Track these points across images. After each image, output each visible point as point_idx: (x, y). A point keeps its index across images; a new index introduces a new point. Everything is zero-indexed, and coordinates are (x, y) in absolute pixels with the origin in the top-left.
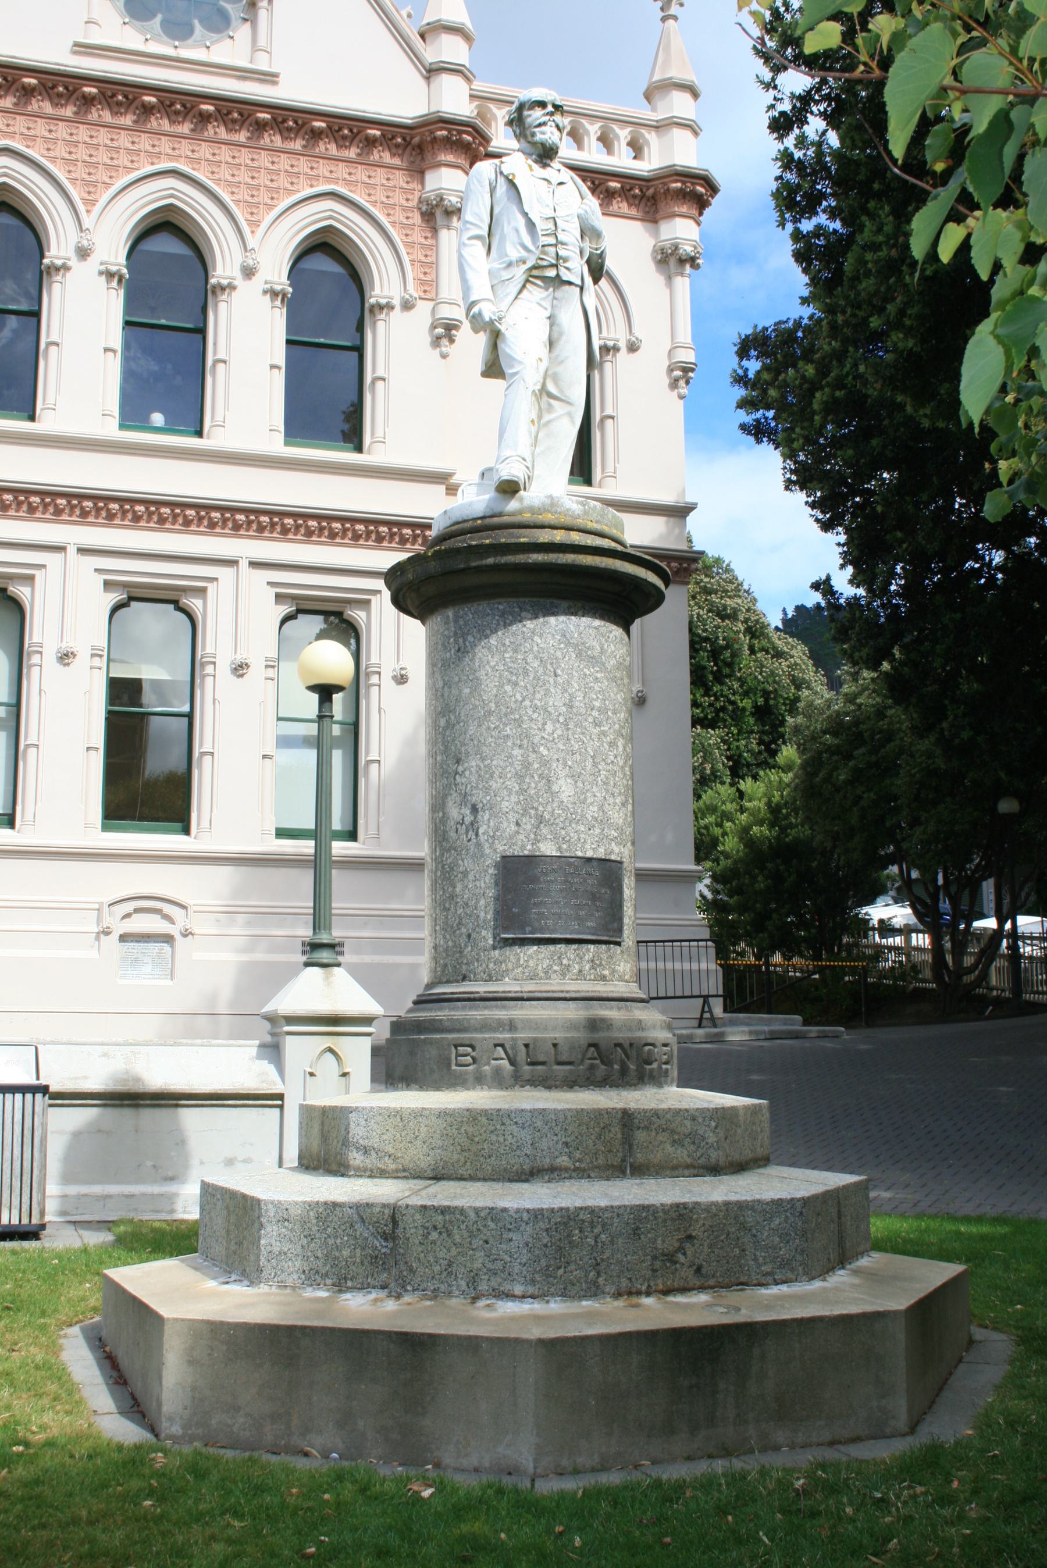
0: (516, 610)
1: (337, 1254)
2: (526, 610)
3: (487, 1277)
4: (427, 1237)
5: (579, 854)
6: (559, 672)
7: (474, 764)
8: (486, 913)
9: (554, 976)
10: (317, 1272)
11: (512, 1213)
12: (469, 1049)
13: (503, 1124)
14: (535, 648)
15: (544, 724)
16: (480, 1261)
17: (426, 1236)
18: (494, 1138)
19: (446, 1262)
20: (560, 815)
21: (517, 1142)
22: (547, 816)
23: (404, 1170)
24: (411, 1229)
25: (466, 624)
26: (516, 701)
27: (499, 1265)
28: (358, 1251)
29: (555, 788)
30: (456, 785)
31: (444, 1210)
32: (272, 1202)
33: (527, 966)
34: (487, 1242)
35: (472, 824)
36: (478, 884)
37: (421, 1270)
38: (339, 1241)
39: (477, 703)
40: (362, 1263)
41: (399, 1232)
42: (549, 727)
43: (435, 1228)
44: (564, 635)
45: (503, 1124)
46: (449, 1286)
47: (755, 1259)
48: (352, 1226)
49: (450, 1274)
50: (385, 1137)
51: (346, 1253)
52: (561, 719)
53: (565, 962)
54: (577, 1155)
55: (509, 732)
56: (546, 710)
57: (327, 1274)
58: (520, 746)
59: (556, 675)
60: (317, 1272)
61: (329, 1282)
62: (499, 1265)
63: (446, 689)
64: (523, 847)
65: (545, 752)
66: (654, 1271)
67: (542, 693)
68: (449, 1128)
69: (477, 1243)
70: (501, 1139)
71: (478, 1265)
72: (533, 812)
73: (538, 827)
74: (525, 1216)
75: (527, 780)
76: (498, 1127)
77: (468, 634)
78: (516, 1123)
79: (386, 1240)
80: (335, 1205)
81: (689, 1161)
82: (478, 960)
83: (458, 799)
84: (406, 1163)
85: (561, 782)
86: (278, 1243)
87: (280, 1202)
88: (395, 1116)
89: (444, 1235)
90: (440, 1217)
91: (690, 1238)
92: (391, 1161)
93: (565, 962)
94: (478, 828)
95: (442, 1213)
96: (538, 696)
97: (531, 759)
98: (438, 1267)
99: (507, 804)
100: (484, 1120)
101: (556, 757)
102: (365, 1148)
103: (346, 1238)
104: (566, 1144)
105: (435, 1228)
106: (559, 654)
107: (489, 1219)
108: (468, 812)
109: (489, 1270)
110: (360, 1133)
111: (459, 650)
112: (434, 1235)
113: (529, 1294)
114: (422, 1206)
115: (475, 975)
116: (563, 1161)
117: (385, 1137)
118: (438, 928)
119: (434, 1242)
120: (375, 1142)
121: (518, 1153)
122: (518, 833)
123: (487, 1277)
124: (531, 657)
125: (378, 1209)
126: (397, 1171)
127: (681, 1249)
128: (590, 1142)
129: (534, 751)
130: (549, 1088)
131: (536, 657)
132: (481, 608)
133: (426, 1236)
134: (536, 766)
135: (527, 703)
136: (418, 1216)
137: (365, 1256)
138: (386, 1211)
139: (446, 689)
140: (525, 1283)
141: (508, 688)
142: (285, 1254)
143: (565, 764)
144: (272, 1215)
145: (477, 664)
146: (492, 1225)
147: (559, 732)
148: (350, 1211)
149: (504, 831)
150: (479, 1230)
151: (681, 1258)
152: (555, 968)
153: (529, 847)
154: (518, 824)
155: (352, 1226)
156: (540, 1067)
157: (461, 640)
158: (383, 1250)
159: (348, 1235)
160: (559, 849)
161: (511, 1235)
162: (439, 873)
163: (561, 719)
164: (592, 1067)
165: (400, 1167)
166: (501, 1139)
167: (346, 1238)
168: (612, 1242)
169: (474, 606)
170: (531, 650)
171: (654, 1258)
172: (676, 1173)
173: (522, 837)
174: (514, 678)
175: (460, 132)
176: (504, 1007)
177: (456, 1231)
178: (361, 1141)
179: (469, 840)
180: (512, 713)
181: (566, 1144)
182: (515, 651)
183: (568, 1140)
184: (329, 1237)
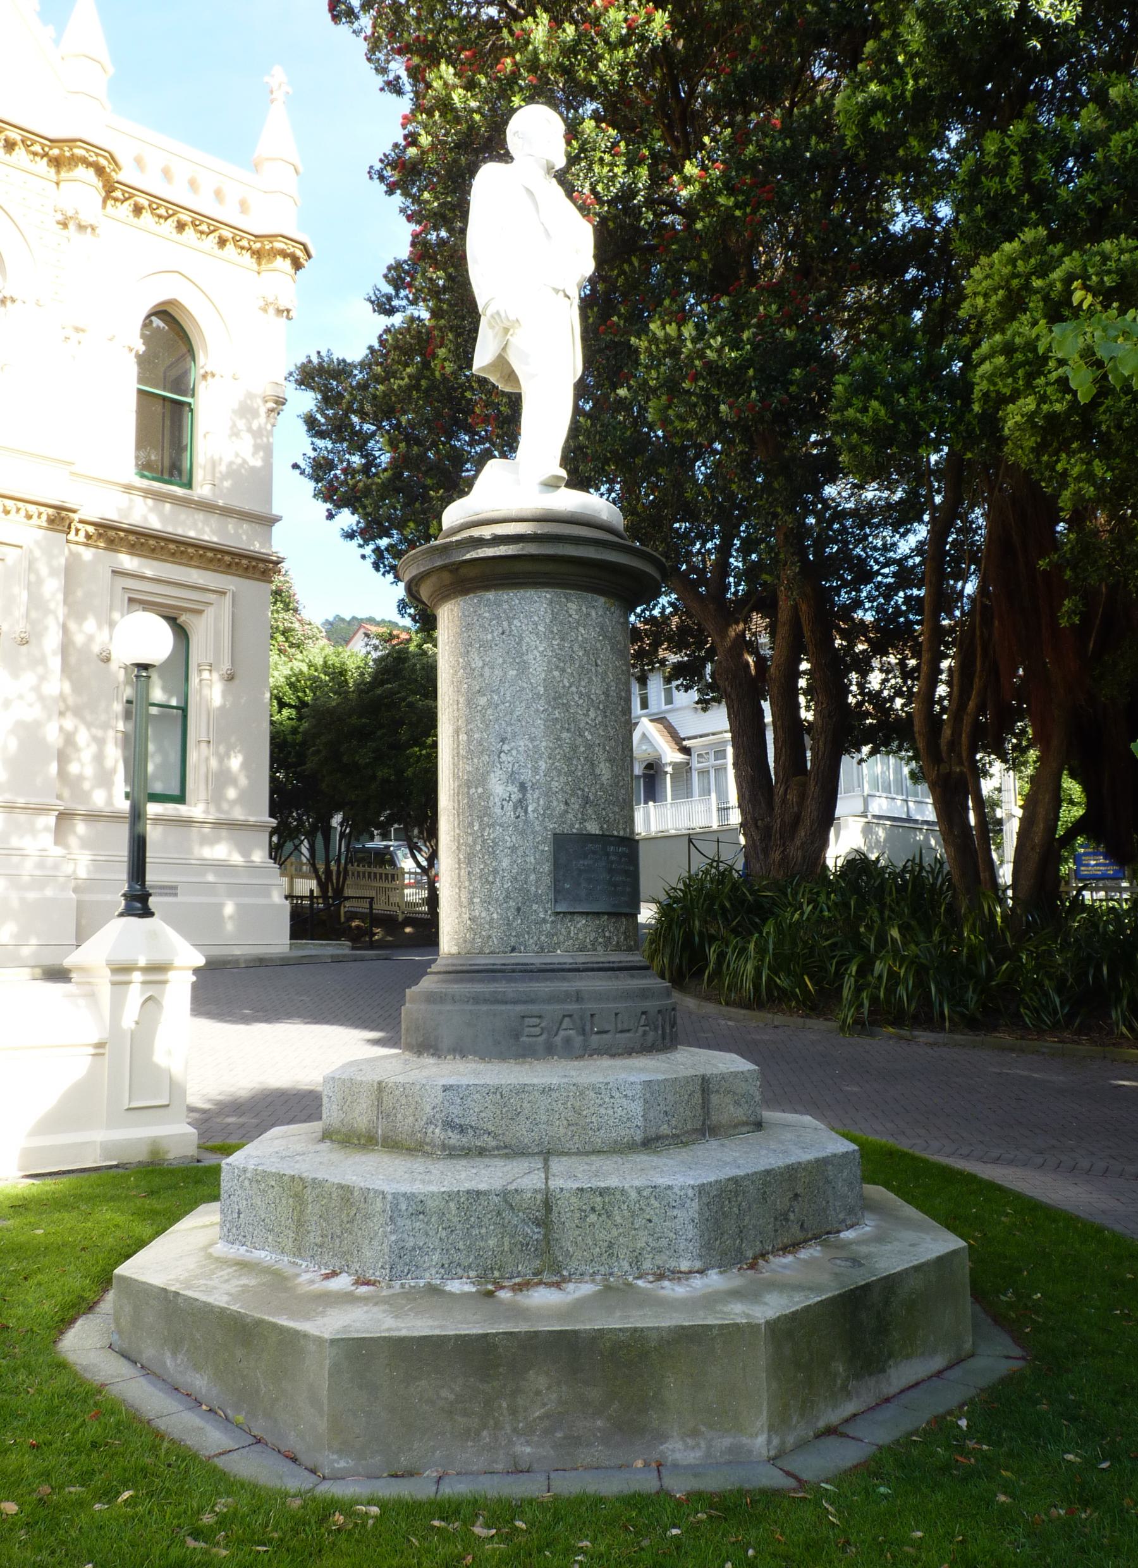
0: (563, 600)
1: (482, 1244)
2: (571, 601)
3: (651, 1256)
4: (585, 1220)
5: (615, 833)
6: (599, 662)
7: (522, 743)
8: (537, 887)
9: (599, 948)
10: (459, 1265)
11: (676, 1190)
12: (537, 1021)
13: (612, 1097)
14: (580, 638)
15: (588, 710)
16: (644, 1239)
17: (583, 1219)
18: (603, 1111)
19: (606, 1244)
20: (601, 797)
21: (627, 1114)
22: (592, 797)
23: (506, 1147)
24: (566, 1212)
25: (512, 608)
26: (564, 686)
27: (664, 1243)
28: (506, 1239)
29: (598, 771)
30: (500, 763)
31: (603, 1192)
32: (404, 1195)
33: (577, 939)
34: (650, 1221)
35: (520, 801)
36: (528, 859)
37: (579, 1254)
38: (483, 1231)
39: (525, 685)
40: (511, 1252)
41: (554, 1217)
42: (592, 714)
43: (593, 1209)
44: (602, 628)
45: (612, 1097)
46: (610, 1268)
47: (835, 1210)
48: (499, 1214)
49: (611, 1255)
50: (483, 1115)
51: (492, 1242)
52: (601, 707)
53: (607, 934)
54: (674, 1123)
55: (557, 715)
56: (589, 697)
57: (469, 1266)
58: (568, 730)
59: (597, 665)
60: (459, 1265)
61: (472, 1274)
62: (664, 1243)
63: (486, 669)
64: (572, 826)
65: (589, 737)
66: (776, 1231)
67: (586, 680)
68: (554, 1104)
69: (639, 1222)
70: (610, 1112)
71: (641, 1244)
72: (580, 792)
73: (584, 807)
74: (690, 1192)
75: (575, 762)
76: (607, 1100)
77: (514, 618)
78: (626, 1096)
79: (538, 1225)
80: (478, 1193)
81: (744, 1119)
82: (528, 933)
83: (504, 777)
84: (507, 1139)
85: (602, 765)
86: (412, 1239)
87: (413, 1194)
88: (495, 1093)
89: (604, 1217)
90: (599, 1199)
91: (796, 1195)
92: (490, 1138)
93: (607, 934)
94: (527, 806)
95: (601, 1195)
96: (583, 683)
97: (577, 743)
98: (598, 1249)
99: (556, 784)
100: (592, 1095)
101: (597, 742)
102: (461, 1126)
103: (492, 1227)
104: (666, 1112)
105: (593, 1209)
106: (598, 645)
107: (652, 1199)
108: (516, 790)
109: (653, 1248)
110: (456, 1112)
111: (503, 633)
112: (593, 1218)
113: (696, 1269)
114: (578, 1189)
115: (525, 947)
116: (665, 1129)
117: (483, 1115)
118: (477, 900)
119: (592, 1225)
120: (472, 1120)
121: (628, 1125)
122: (567, 812)
123: (651, 1256)
124: (576, 646)
125: (529, 1196)
126: (498, 1148)
127: (791, 1209)
128: (682, 1110)
129: (580, 735)
130: (613, 1056)
131: (581, 647)
132: (528, 595)
133: (583, 1219)
134: (582, 749)
135: (574, 689)
136: (573, 1200)
137: (515, 1244)
138: (539, 1197)
139: (486, 669)
140: (692, 1259)
141: (556, 673)
142: (420, 1248)
143: (604, 749)
144: (404, 1208)
145: (524, 648)
146: (656, 1204)
147: (600, 719)
148: (496, 1199)
149: (554, 810)
150: (641, 1209)
151: (792, 1216)
152: (600, 940)
153: (577, 826)
154: (567, 804)
155: (499, 1214)
156: (605, 1036)
157: (505, 624)
158: (535, 1237)
159: (495, 1224)
160: (601, 828)
161: (675, 1212)
162: (478, 847)
163: (601, 707)
164: (645, 1033)
165: (502, 1144)
166: (610, 1112)
167: (492, 1227)
168: (749, 1208)
169: (521, 593)
170: (576, 639)
171: (776, 1219)
172: (737, 1131)
173: (570, 816)
174: (562, 665)
175: (97, 155)
176: (564, 979)
177: (616, 1212)
178: (457, 1120)
179: (518, 817)
180: (560, 698)
181: (666, 1112)
182: (563, 639)
183: (668, 1109)
184: (472, 1227)
